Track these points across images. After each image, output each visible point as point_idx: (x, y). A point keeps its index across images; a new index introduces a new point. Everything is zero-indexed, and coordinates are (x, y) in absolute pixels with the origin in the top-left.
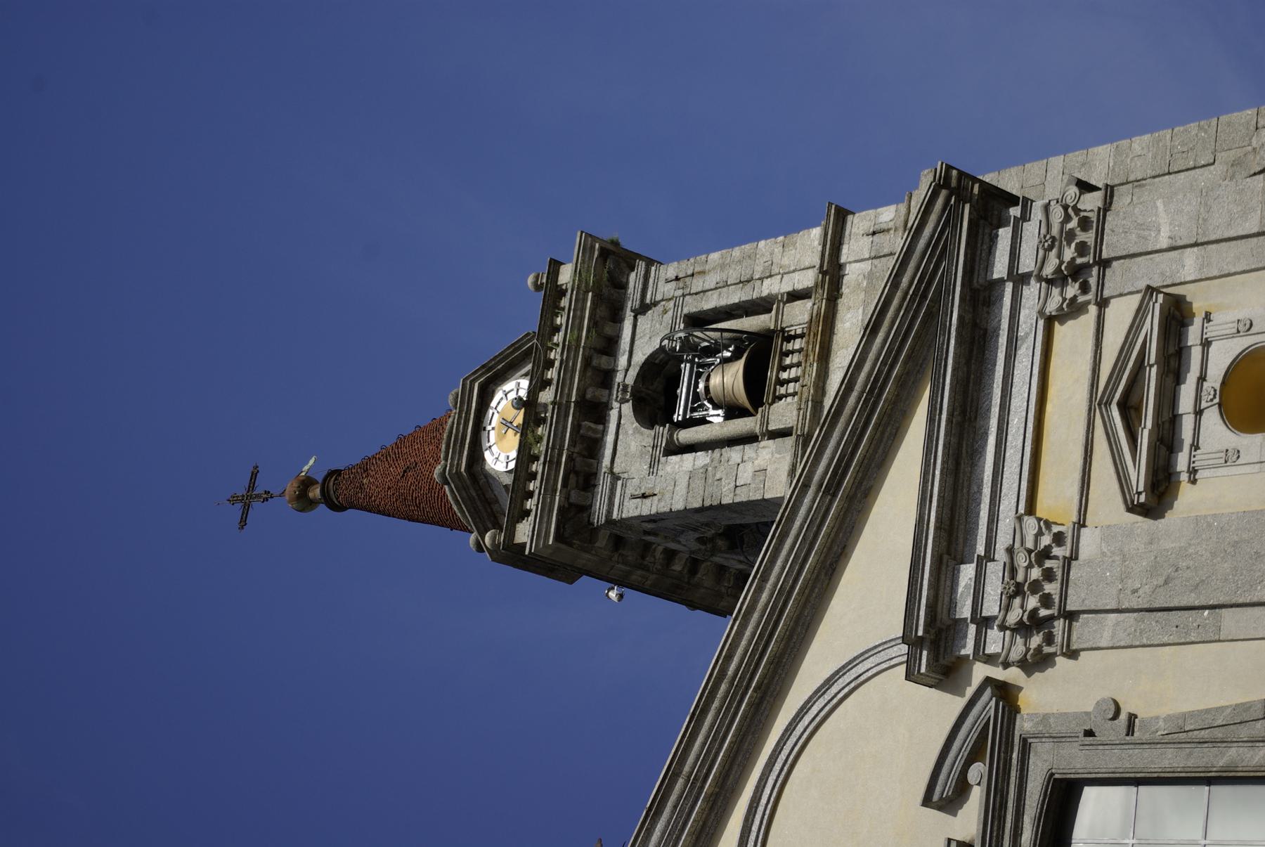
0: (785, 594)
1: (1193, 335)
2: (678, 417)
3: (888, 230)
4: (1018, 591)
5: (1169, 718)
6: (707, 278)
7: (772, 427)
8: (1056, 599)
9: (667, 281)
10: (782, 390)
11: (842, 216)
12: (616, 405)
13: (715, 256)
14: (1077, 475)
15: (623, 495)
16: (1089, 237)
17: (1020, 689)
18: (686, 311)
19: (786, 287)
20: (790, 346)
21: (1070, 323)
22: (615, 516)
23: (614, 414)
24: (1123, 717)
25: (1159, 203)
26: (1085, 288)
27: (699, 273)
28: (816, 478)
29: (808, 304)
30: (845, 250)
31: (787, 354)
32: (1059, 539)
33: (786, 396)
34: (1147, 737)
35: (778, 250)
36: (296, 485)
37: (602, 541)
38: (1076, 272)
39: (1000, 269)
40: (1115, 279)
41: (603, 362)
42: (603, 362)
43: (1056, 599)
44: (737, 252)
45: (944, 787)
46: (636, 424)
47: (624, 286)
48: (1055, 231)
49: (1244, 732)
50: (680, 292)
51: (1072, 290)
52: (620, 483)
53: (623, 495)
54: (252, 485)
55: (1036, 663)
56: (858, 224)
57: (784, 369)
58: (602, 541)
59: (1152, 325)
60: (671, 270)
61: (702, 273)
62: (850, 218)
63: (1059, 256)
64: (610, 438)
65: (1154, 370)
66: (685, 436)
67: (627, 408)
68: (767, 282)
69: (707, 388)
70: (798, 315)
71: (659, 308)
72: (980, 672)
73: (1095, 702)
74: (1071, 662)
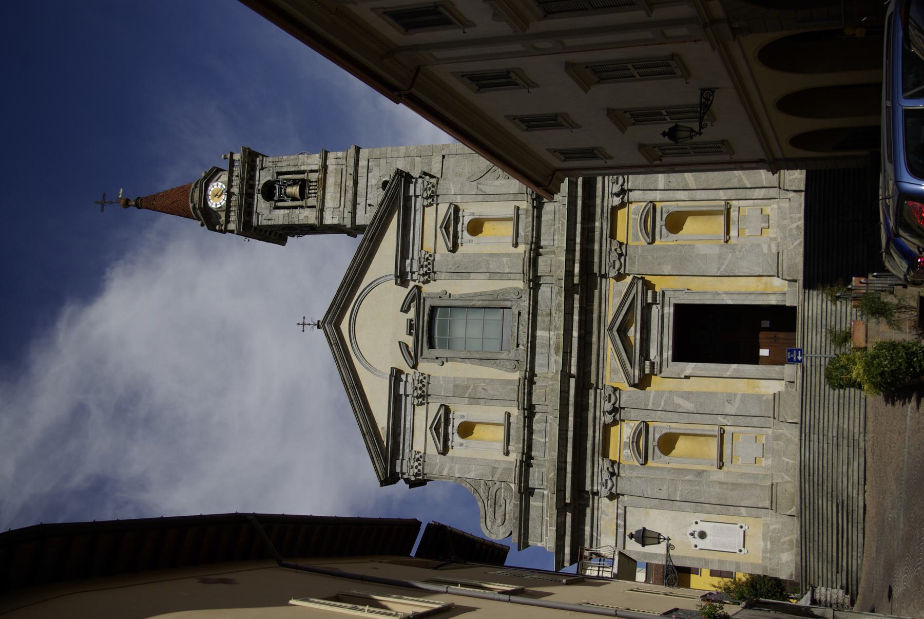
0: (360, 264)
1: (461, 214)
2: (276, 198)
3: (340, 158)
4: (422, 266)
5: (458, 295)
6: (283, 163)
7: (308, 205)
8: (431, 269)
9: (269, 162)
10: (310, 195)
11: (326, 153)
12: (256, 194)
13: (285, 157)
14: (433, 242)
15: (262, 219)
16: (434, 189)
17: (422, 287)
18: (276, 171)
19: (309, 168)
20: (311, 184)
21: (429, 207)
22: (260, 224)
23: (256, 197)
24: (448, 294)
25: (451, 184)
26: (433, 200)
27: (280, 161)
28: (367, 238)
29: (317, 174)
30: (328, 161)
31: (311, 186)
32: (430, 256)
33: (311, 197)
34: (454, 298)
35: (306, 159)
36: (124, 201)
37: (253, 229)
38: (431, 197)
39: (411, 193)
40: (440, 199)
41: (251, 182)
42: (251, 182)
43: (431, 269)
44: (292, 157)
45: (405, 308)
46: (263, 200)
47: (256, 162)
48: (425, 187)
49: (476, 298)
50: (274, 166)
51: (430, 201)
52: (260, 216)
53: (262, 219)
54: (104, 199)
55: (427, 282)
56: (331, 155)
57: (310, 190)
58: (253, 229)
59: (452, 210)
60: (270, 159)
61: (281, 161)
62: (328, 153)
63: (427, 193)
64: (255, 203)
65: (452, 221)
66: (279, 204)
67: (260, 196)
68: (302, 166)
69: (285, 192)
70: (314, 177)
71: (268, 169)
72: (412, 284)
73: (172, 188)
74: (434, 282)
